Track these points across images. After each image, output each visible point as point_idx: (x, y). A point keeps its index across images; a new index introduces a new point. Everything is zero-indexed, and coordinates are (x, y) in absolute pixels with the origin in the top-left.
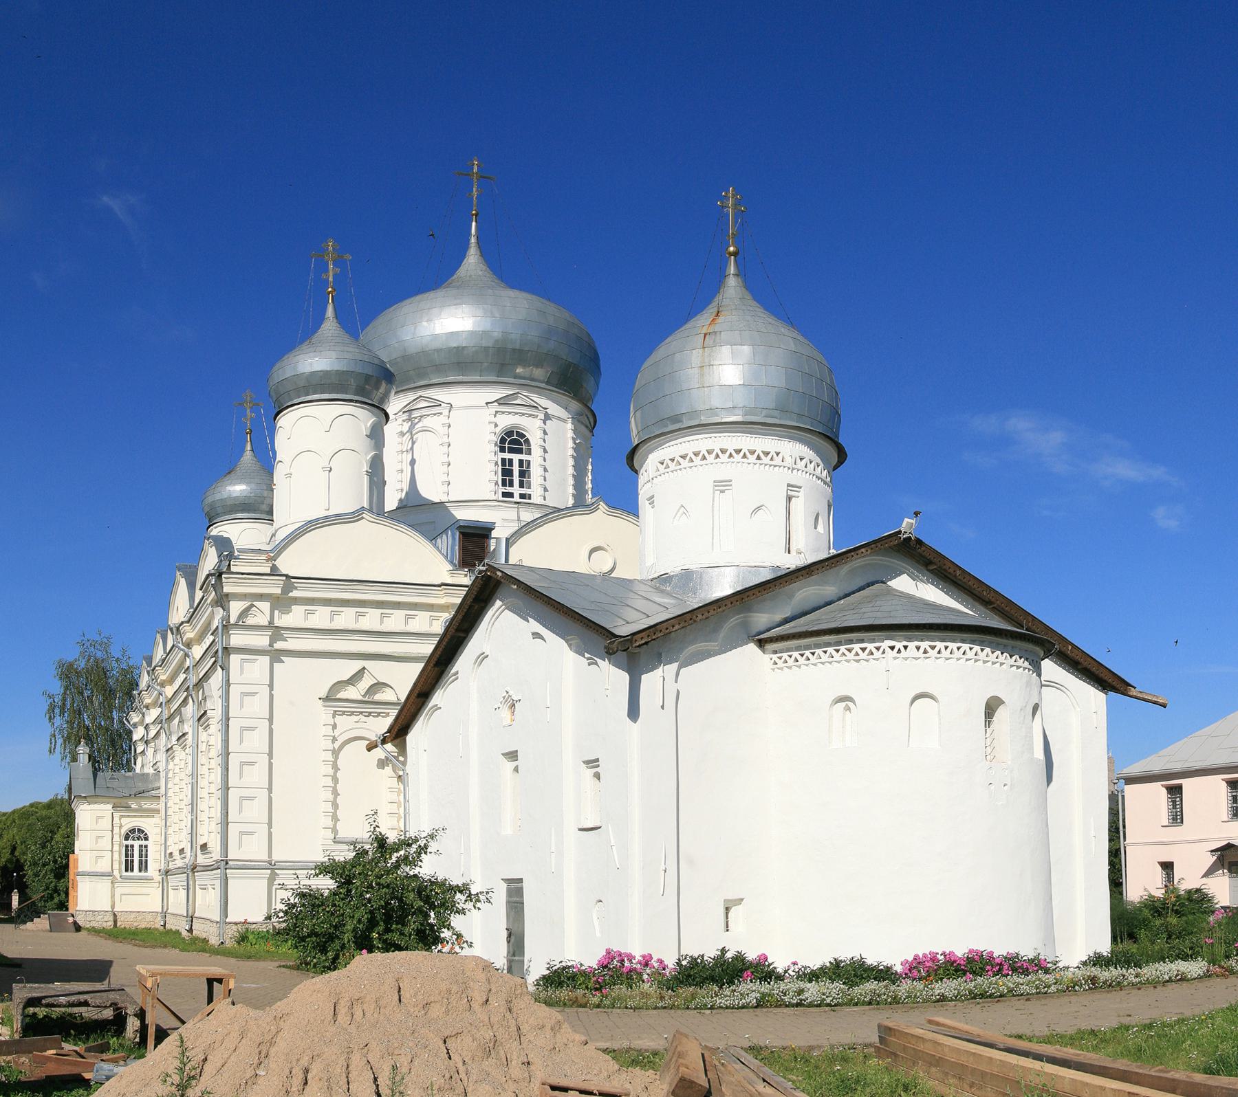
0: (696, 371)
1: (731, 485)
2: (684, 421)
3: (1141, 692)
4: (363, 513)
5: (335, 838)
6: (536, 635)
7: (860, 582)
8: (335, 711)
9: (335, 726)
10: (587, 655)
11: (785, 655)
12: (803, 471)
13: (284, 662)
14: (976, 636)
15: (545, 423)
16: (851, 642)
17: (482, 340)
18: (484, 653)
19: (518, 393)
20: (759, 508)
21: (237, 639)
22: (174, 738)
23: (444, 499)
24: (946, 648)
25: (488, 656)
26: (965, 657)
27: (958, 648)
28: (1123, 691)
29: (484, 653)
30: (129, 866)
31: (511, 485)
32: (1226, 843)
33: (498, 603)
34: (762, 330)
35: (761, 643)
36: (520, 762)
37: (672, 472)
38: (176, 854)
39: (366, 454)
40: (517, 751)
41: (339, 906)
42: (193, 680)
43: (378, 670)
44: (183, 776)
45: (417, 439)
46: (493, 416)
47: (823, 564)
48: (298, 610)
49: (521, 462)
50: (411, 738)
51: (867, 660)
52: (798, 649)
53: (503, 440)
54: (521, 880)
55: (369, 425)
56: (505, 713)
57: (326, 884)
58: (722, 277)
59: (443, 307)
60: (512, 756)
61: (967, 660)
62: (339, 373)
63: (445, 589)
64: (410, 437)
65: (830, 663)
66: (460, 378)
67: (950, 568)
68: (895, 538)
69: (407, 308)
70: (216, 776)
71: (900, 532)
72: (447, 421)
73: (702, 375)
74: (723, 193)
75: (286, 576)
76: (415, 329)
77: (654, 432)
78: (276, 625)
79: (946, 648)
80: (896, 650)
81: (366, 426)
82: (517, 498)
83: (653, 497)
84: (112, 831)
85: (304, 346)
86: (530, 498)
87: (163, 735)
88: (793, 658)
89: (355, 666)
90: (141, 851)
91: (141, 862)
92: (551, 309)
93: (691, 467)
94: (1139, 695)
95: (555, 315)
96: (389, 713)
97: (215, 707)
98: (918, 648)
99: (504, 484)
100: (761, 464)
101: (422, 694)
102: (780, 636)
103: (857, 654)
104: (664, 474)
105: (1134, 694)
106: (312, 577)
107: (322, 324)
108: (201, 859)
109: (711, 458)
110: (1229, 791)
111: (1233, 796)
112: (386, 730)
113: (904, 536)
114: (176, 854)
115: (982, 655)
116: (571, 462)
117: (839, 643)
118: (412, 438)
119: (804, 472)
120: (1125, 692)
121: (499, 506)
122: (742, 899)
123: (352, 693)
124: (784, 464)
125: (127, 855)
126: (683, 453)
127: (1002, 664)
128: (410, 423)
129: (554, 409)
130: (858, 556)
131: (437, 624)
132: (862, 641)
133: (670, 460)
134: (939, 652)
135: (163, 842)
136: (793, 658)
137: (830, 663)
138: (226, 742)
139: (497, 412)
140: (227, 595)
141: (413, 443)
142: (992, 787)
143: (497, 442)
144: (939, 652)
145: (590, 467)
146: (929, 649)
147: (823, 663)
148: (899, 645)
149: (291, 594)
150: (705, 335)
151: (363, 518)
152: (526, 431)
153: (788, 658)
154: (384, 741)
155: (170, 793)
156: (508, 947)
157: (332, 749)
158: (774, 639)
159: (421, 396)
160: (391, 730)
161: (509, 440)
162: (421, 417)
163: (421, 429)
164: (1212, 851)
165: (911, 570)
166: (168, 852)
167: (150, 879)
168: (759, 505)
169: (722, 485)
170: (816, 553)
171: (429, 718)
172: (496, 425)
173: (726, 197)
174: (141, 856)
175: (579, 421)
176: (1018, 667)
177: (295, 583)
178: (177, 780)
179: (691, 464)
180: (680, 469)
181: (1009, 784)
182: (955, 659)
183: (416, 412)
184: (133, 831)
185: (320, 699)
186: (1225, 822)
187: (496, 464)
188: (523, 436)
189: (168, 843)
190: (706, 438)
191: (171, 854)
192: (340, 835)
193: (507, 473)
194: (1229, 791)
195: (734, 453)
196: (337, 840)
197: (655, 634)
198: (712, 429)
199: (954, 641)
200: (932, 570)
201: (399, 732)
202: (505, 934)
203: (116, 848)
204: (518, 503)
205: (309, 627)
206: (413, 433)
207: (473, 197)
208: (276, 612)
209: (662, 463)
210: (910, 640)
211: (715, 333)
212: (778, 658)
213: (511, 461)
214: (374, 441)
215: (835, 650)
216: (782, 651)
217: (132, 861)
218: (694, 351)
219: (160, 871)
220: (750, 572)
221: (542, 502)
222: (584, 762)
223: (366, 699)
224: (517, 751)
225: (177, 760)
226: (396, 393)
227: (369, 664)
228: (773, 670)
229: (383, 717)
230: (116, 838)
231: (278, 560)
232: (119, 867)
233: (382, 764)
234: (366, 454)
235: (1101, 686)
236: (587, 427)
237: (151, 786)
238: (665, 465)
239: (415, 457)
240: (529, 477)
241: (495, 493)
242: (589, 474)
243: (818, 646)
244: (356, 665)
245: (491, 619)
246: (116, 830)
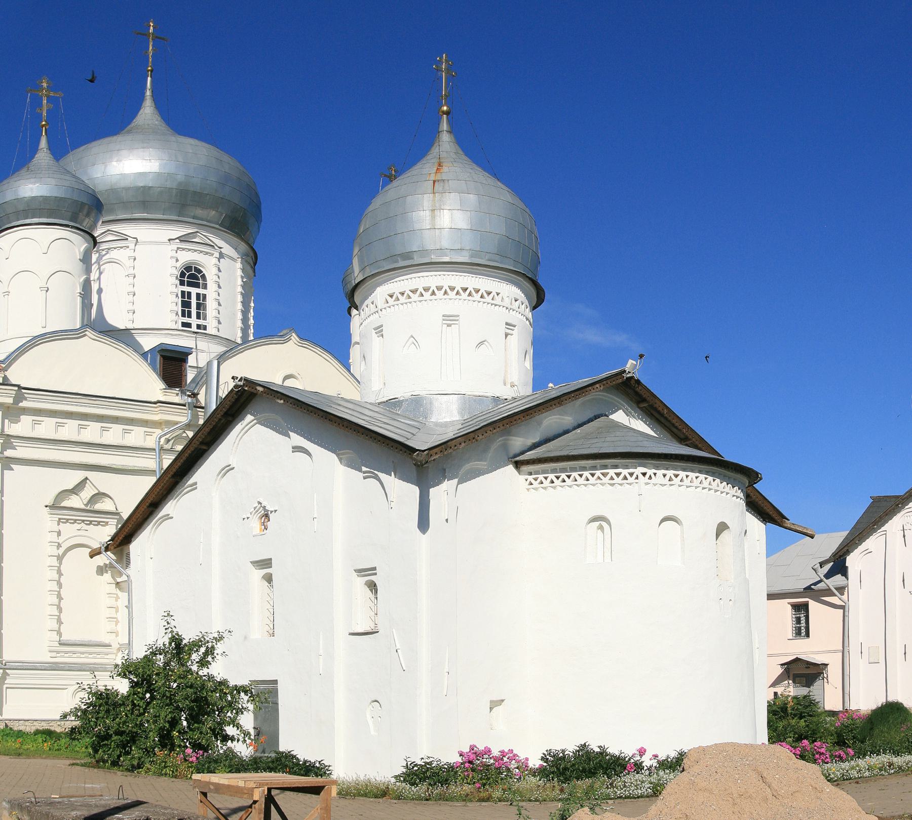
0: (428, 213)
2: (415, 258)
3: (794, 524)
4: (86, 331)
5: (60, 641)
6: (297, 449)
7: (589, 414)
8: (60, 519)
9: (59, 533)
10: (364, 469)
11: (541, 477)
12: (517, 312)
13: (13, 470)
14: (690, 465)
15: (219, 261)
16: (605, 467)
17: (166, 181)
18: (230, 465)
19: (197, 232)
20: (482, 343)
23: (130, 326)
24: (687, 476)
25: (234, 468)
26: (702, 486)
27: (697, 478)
28: (780, 522)
29: (230, 465)
31: (190, 316)
32: (794, 657)
33: (249, 418)
34: (484, 182)
35: (518, 465)
37: (402, 304)
39: (80, 277)
40: (271, 559)
41: (138, 705)
43: (101, 481)
45: (104, 269)
46: (175, 251)
47: (570, 396)
48: (26, 420)
49: (198, 295)
50: (136, 547)
51: (621, 485)
52: (554, 471)
53: (182, 275)
54: (275, 682)
55: (82, 249)
56: (255, 524)
57: (122, 686)
58: (437, 132)
59: (131, 149)
60: (265, 563)
61: (704, 488)
62: (45, 199)
63: (161, 406)
64: (97, 267)
65: (585, 485)
66: (145, 215)
67: (659, 406)
68: (620, 376)
69: (96, 148)
71: (625, 371)
72: (133, 254)
73: (433, 217)
74: (438, 58)
75: (18, 386)
76: (105, 168)
77: (384, 267)
78: (6, 433)
80: (648, 476)
81: (79, 251)
82: (194, 328)
83: (382, 326)
85: (23, 172)
88: (549, 480)
89: (77, 476)
92: (226, 158)
93: (420, 301)
94: (792, 527)
95: (229, 164)
96: (108, 522)
98: (664, 476)
99: (183, 315)
100: (484, 303)
102: (538, 459)
103: (612, 478)
104: (393, 306)
105: (789, 526)
107: (35, 155)
109: (440, 294)
110: (794, 613)
111: (796, 618)
113: (628, 376)
115: (714, 484)
116: (239, 298)
117: (594, 468)
118: (99, 268)
119: (518, 313)
120: (781, 524)
121: (180, 335)
122: (503, 701)
123: (75, 502)
126: (413, 288)
127: (727, 493)
128: (98, 254)
129: (227, 249)
130: (595, 390)
132: (616, 467)
133: (400, 293)
136: (549, 480)
137: (585, 485)
139: (178, 248)
141: (101, 273)
142: (722, 602)
143: (177, 276)
144: (637, 478)
145: (252, 305)
146: (673, 477)
148: (650, 472)
149: (21, 404)
150: (434, 182)
151: (85, 335)
152: (203, 267)
153: (544, 480)
154: (107, 549)
157: (57, 555)
159: (109, 230)
160: (115, 537)
161: (188, 274)
162: (109, 249)
163: (108, 260)
165: (626, 406)
168: (483, 340)
169: (450, 320)
170: (525, 387)
171: (156, 528)
172: (177, 260)
173: (441, 62)
175: (246, 261)
177: (26, 393)
179: (421, 298)
180: (410, 303)
181: (733, 600)
182: (694, 488)
183: (104, 244)
185: (46, 506)
186: (791, 639)
187: (177, 296)
188: (200, 271)
190: (436, 276)
192: (65, 637)
193: (186, 304)
194: (794, 613)
195: (461, 291)
196: (62, 642)
197: (446, 450)
198: (461, 268)
199: (692, 471)
200: (642, 408)
204: (196, 333)
205: (36, 437)
206: (101, 264)
207: (148, 55)
208: (6, 421)
209: (391, 296)
210: (657, 468)
211: (444, 180)
212: (534, 479)
213: (189, 294)
214: (85, 265)
215: (591, 474)
216: (537, 473)
218: (425, 195)
220: (475, 401)
221: (217, 334)
222: (355, 570)
223: (88, 508)
224: (271, 559)
226: (103, 222)
227: (91, 475)
228: (528, 490)
229: (102, 525)
231: (9, 370)
233: (101, 570)
234: (79, 277)
235: (762, 518)
239: (101, 286)
241: (176, 322)
242: (252, 311)
243: (574, 469)
244: (79, 475)
245: (240, 432)
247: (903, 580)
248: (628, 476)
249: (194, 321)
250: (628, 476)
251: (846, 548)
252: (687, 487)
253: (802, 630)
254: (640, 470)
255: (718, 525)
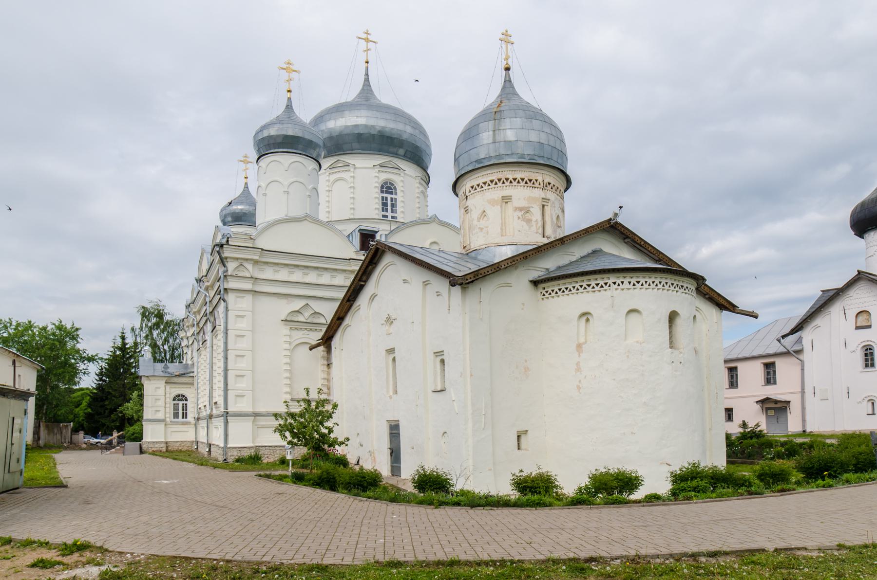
1: (511, 199)
21: (232, 284)
22: (201, 343)
30: (176, 415)
36: (397, 354)
38: (202, 408)
40: (394, 348)
42: (209, 310)
43: (317, 306)
44: (205, 364)
49: (392, 199)
50: (335, 343)
51: (600, 291)
53: (382, 187)
61: (658, 289)
70: (221, 364)
79: (646, 282)
80: (617, 284)
82: (390, 218)
84: (165, 396)
86: (397, 219)
87: (196, 343)
90: (183, 407)
91: (183, 413)
93: (489, 189)
97: (220, 321)
98: (630, 283)
99: (383, 210)
101: (339, 318)
106: (277, 250)
108: (215, 412)
112: (320, 338)
114: (202, 408)
124: (539, 186)
125: (174, 410)
127: (677, 291)
131: (346, 281)
134: (642, 285)
135: (196, 402)
138: (226, 343)
140: (226, 258)
142: (673, 364)
146: (636, 283)
147: (573, 294)
148: (618, 281)
152: (394, 182)
155: (199, 375)
156: (391, 459)
158: (543, 281)
164: (757, 402)
166: (199, 407)
167: (189, 423)
169: (506, 199)
174: (183, 410)
176: (686, 293)
178: (202, 367)
182: (645, 289)
184: (178, 396)
188: (391, 183)
189: (199, 402)
191: (200, 408)
193: (384, 204)
201: (327, 340)
202: (389, 451)
203: (168, 405)
213: (386, 198)
217: (178, 413)
219: (194, 418)
225: (202, 356)
227: (312, 303)
230: (168, 400)
232: (170, 417)
236: (425, 182)
237: (189, 371)
238: (474, 188)
240: (396, 207)
246: (168, 395)
247: (812, 346)
248: (604, 285)
249: (389, 214)
250: (604, 285)
251: (800, 325)
252: (646, 289)
253: (770, 379)
254: (612, 280)
255: (670, 313)
